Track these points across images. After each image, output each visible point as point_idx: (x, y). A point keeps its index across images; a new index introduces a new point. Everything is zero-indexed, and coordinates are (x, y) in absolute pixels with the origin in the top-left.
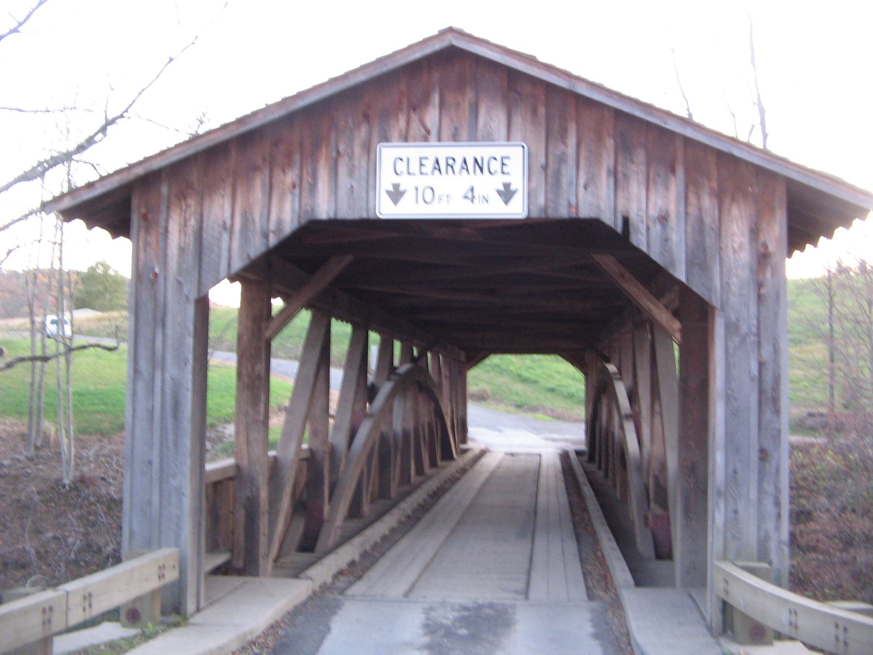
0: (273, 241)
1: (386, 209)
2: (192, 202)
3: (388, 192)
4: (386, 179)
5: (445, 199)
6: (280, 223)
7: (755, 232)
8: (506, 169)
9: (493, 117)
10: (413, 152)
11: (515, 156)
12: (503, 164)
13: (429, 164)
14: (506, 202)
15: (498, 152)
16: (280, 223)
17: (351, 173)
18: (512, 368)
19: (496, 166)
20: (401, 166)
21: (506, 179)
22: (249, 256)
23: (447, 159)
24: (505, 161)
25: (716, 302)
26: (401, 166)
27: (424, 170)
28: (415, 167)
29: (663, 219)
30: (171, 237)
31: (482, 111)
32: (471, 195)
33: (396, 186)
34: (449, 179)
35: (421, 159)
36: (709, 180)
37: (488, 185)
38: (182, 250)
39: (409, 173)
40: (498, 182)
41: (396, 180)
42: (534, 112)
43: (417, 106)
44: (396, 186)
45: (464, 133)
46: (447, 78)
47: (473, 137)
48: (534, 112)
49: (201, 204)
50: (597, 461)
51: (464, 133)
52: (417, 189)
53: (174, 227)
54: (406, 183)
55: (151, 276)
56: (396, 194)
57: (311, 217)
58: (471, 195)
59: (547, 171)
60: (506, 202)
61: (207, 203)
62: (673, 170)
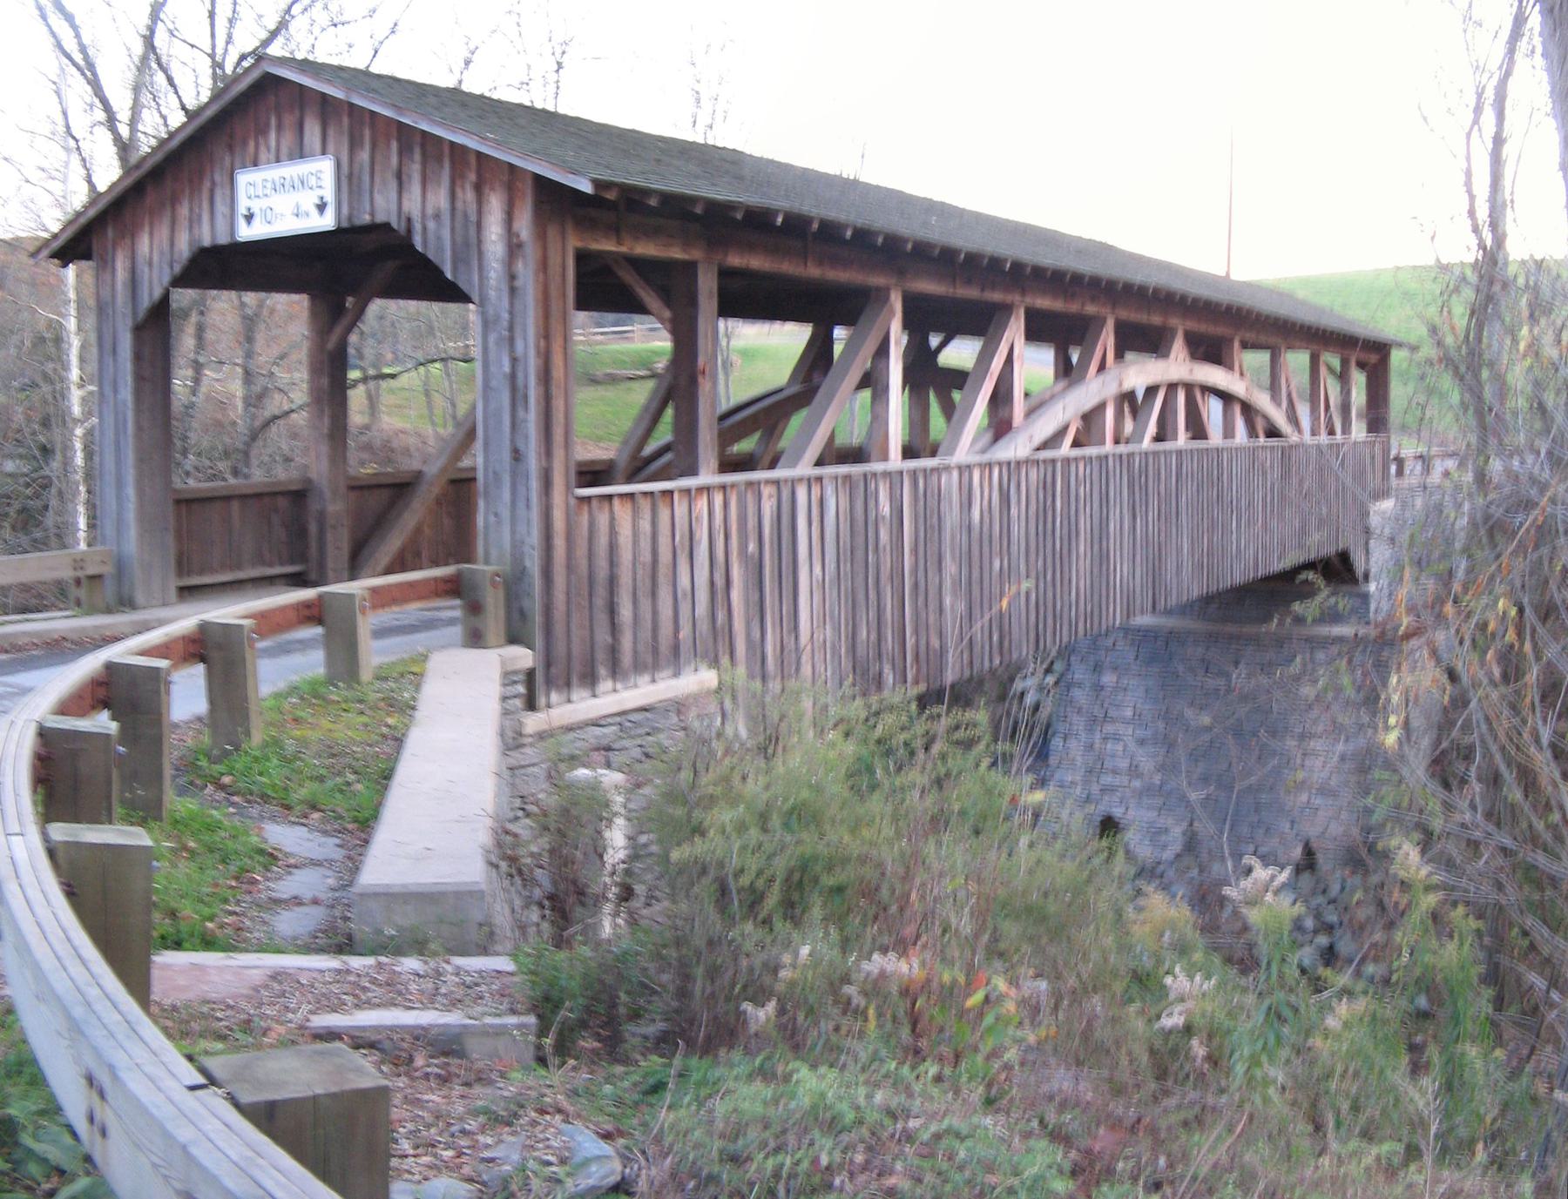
1: (245, 233)
4: (243, 205)
46: (260, 105)
54: (256, 206)
56: (249, 218)
59: (348, 181)
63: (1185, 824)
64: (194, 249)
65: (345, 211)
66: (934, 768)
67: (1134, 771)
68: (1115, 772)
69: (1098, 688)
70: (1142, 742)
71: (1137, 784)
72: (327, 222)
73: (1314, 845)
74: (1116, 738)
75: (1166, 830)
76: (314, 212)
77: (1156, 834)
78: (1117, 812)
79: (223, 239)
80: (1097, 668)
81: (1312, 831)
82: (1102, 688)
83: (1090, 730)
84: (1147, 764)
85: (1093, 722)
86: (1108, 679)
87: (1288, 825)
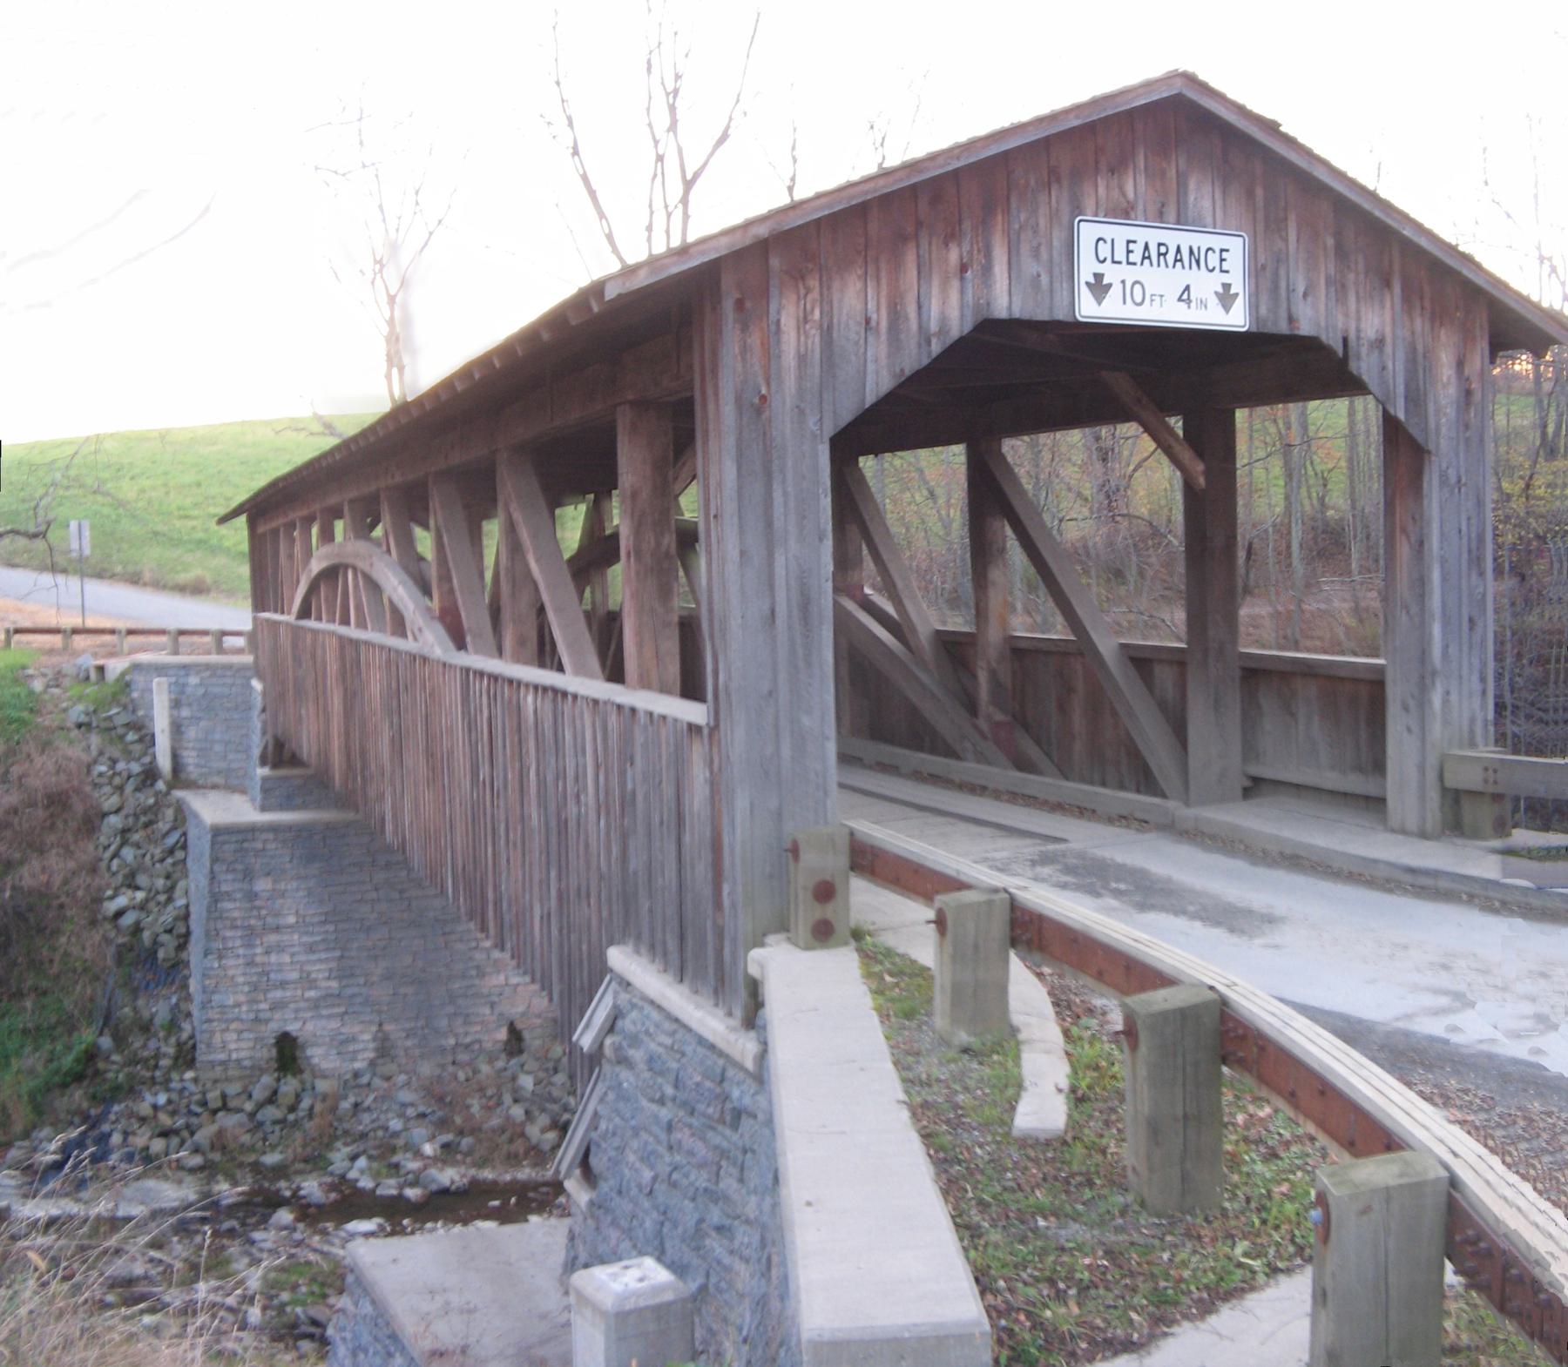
0: (936, 348)
1: (1089, 309)
2: (813, 283)
3: (1087, 284)
4: (1086, 268)
5: (1157, 299)
6: (944, 320)
7: (1460, 364)
8: (1225, 266)
9: (1202, 194)
10: (1119, 233)
11: (1236, 248)
12: (1222, 260)
13: (1138, 250)
14: (1099, 300)
15: (1218, 242)
16: (944, 320)
17: (1036, 253)
18: (227, 544)
19: (1213, 260)
20: (1104, 250)
21: (1226, 278)
22: (902, 370)
23: (1160, 245)
24: (1225, 255)
25: (1431, 447)
26: (1104, 250)
27: (1132, 258)
28: (1120, 255)
29: (1380, 343)
30: (784, 338)
31: (1192, 185)
32: (1185, 296)
33: (1099, 277)
34: (1164, 275)
35: (1129, 242)
36: (960, 245)
37: (1206, 284)
38: (802, 359)
39: (1114, 262)
40: (1215, 282)
41: (1100, 268)
42: (1250, 194)
43: (1117, 168)
44: (1099, 277)
45: (1171, 213)
46: (1177, 139)
47: (1182, 220)
48: (1250, 194)
49: (826, 287)
50: (710, 696)
51: (1171, 213)
52: (1123, 282)
53: (788, 322)
54: (1111, 274)
55: (756, 401)
56: (1099, 287)
57: (985, 315)
58: (1185, 296)
59: (1264, 273)
60: (1099, 300)
61: (836, 285)
62: (1387, 284)
63: (374, 1028)
64: (980, 319)
65: (1263, 310)
66: (742, 1136)
67: (308, 981)
68: (283, 985)
69: (252, 896)
70: (311, 949)
71: (311, 994)
72: (1236, 319)
73: (519, 1026)
74: (280, 948)
75: (353, 1039)
76: (1213, 302)
77: (342, 1044)
78: (293, 1028)
79: (1061, 315)
80: (248, 875)
81: (516, 1009)
82: (256, 895)
83: (250, 946)
84: (319, 970)
85: (250, 935)
86: (263, 885)
87: (487, 1011)
